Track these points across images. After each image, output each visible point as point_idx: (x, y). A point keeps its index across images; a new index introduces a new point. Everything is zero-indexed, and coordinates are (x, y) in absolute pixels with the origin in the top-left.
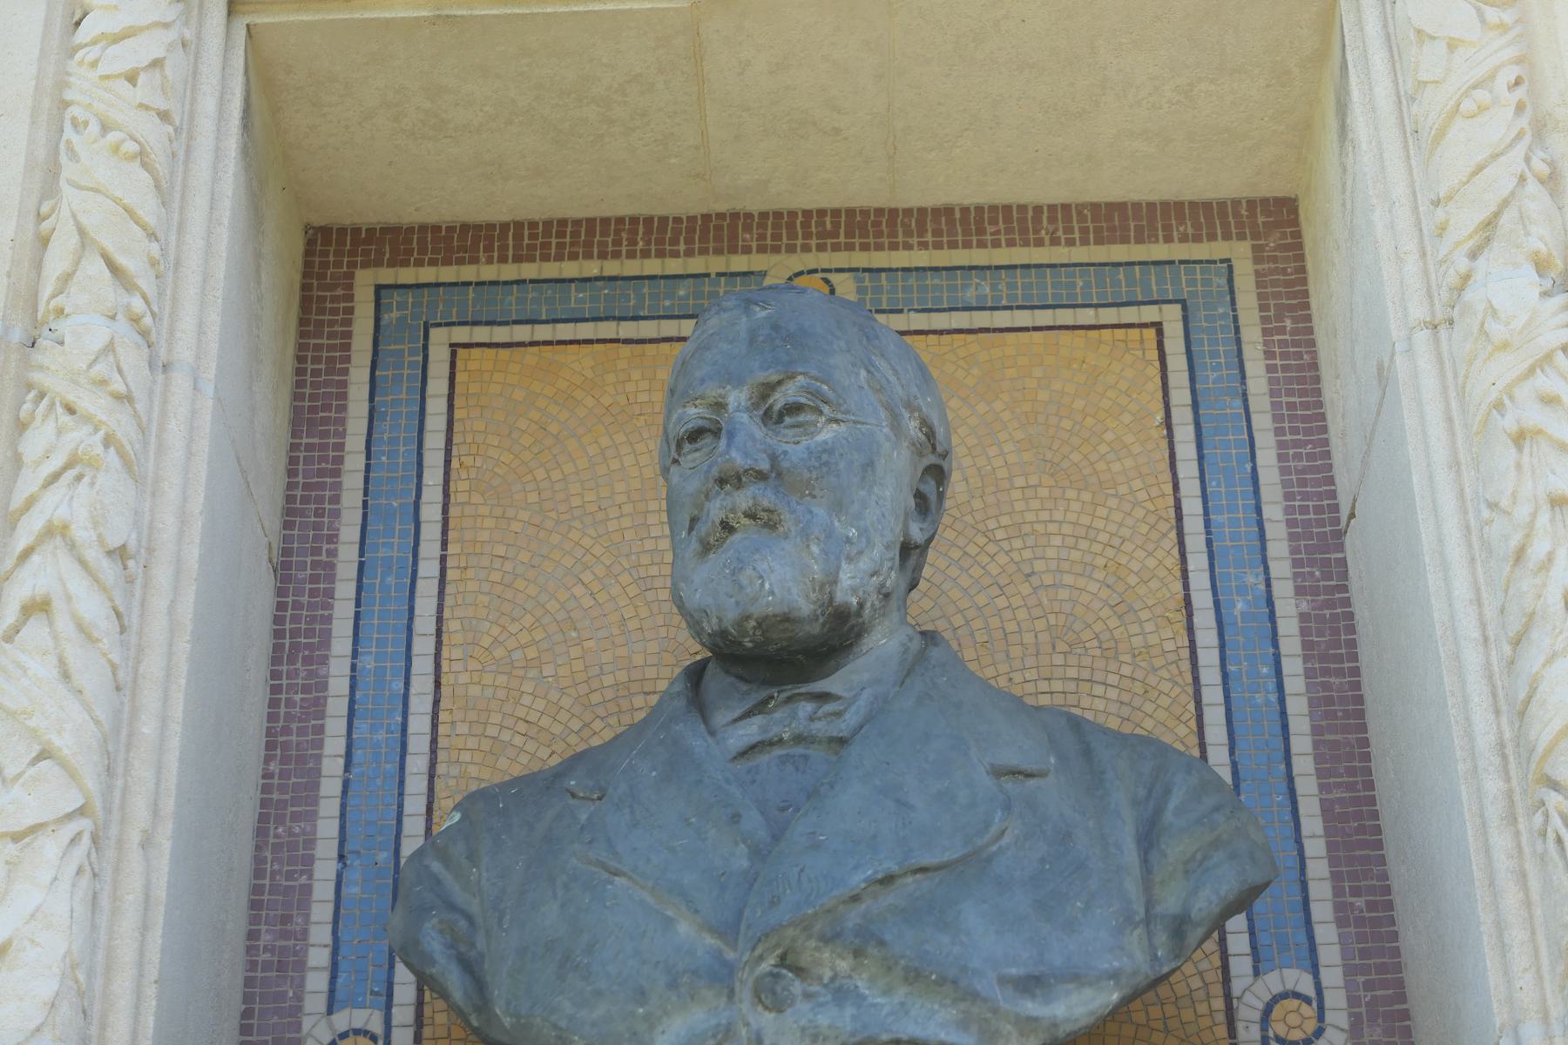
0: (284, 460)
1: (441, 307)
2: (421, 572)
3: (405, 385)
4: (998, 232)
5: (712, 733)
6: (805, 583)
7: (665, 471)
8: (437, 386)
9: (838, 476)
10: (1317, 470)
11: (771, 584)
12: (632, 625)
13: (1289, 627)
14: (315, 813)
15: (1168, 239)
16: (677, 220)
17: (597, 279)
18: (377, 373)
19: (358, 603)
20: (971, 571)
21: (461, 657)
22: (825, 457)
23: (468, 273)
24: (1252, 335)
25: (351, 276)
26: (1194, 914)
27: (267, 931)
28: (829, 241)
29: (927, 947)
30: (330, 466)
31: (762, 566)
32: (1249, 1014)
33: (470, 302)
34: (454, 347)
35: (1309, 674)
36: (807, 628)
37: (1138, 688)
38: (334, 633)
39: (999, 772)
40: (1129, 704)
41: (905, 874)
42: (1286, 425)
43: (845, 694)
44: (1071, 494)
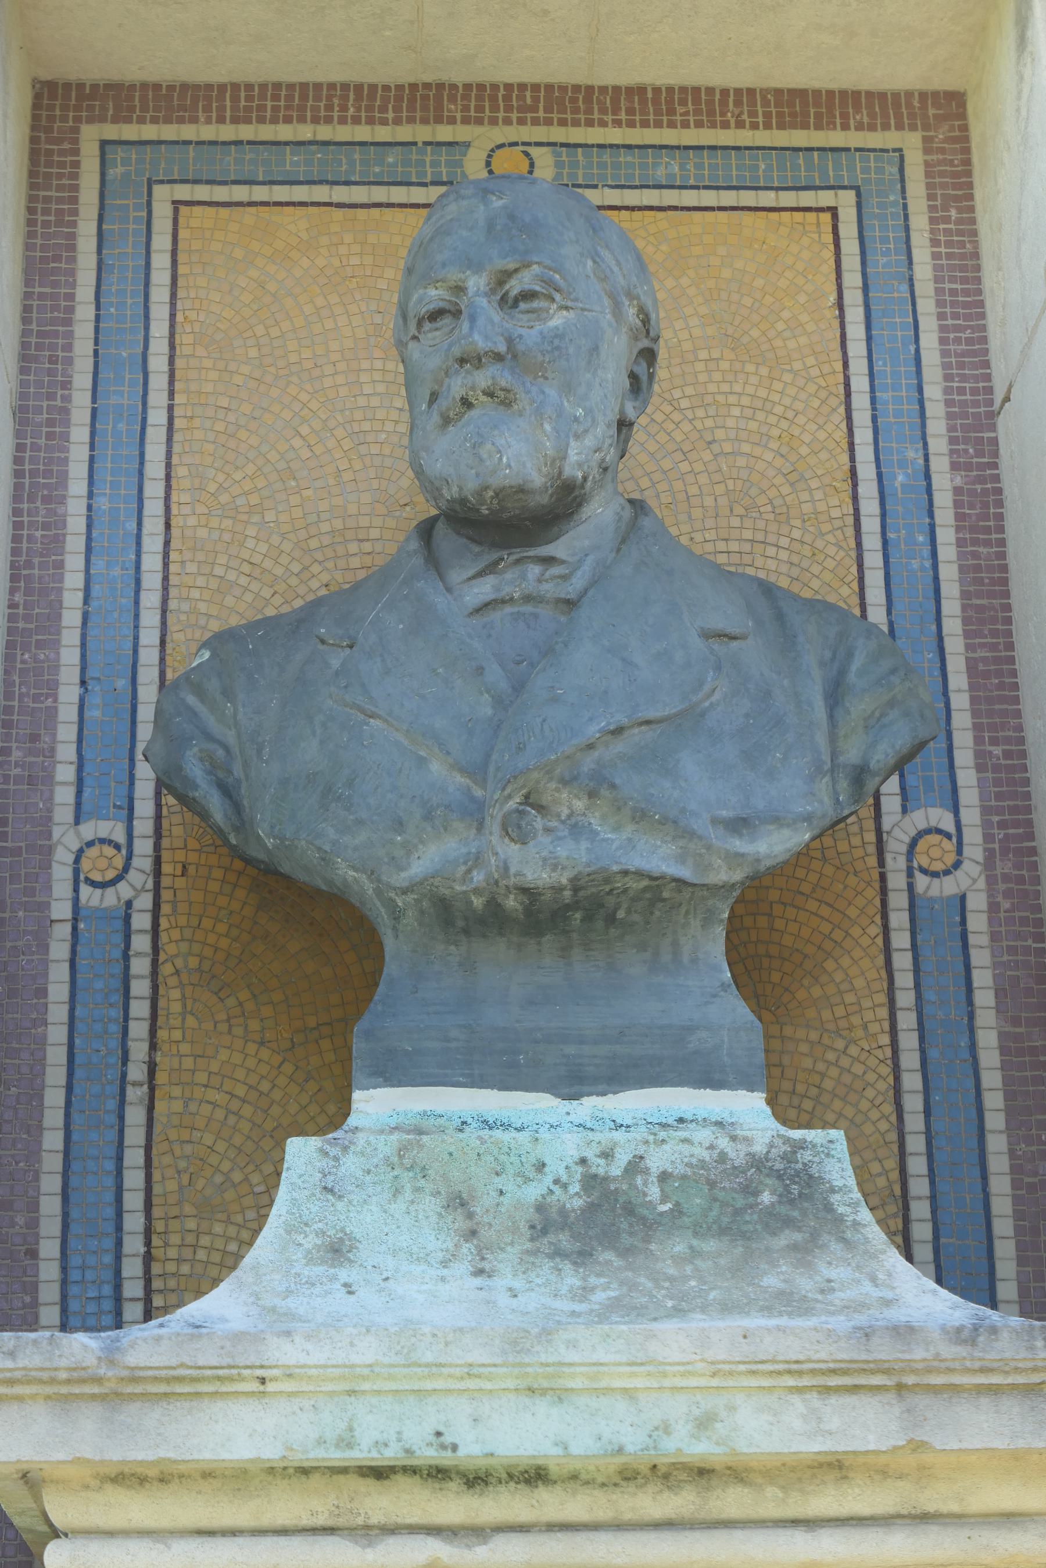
0: (19, 308)
1: (163, 165)
2: (150, 420)
3: (131, 239)
4: (687, 113)
5: (449, 590)
6: (538, 458)
7: (401, 345)
8: (161, 242)
9: (567, 360)
10: (973, 353)
11: (508, 458)
12: (347, 476)
13: (943, 500)
14: (58, 641)
15: (845, 127)
16: (386, 88)
17: (311, 143)
18: (104, 227)
19: (92, 447)
20: (657, 437)
21: (189, 501)
22: (556, 342)
23: (188, 132)
24: (920, 221)
25: (76, 130)
26: (873, 765)
27: (17, 748)
28: (529, 115)
29: (652, 791)
30: (62, 315)
31: (501, 442)
32: (896, 846)
33: (191, 161)
34: (176, 204)
35: (960, 543)
36: (538, 498)
37: (807, 551)
38: (71, 475)
39: (708, 635)
40: (799, 566)
41: (632, 726)
42: (948, 310)
43: (569, 559)
44: (750, 368)
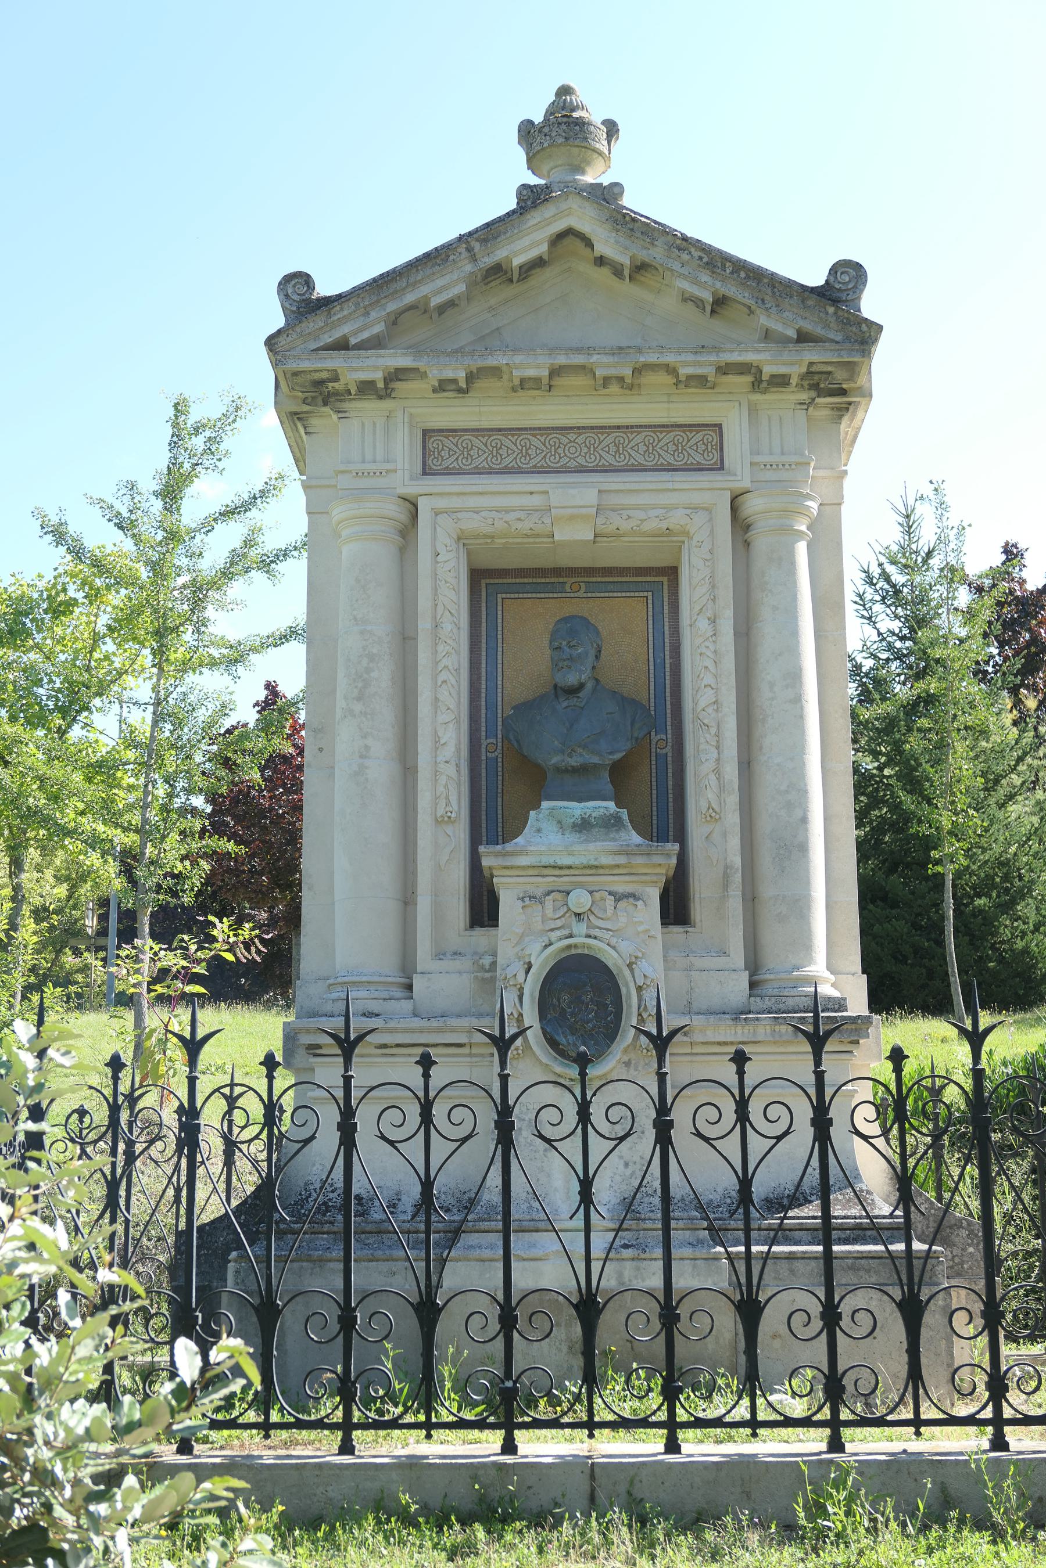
13: (668, 665)
23: (505, 581)
32: (654, 743)
